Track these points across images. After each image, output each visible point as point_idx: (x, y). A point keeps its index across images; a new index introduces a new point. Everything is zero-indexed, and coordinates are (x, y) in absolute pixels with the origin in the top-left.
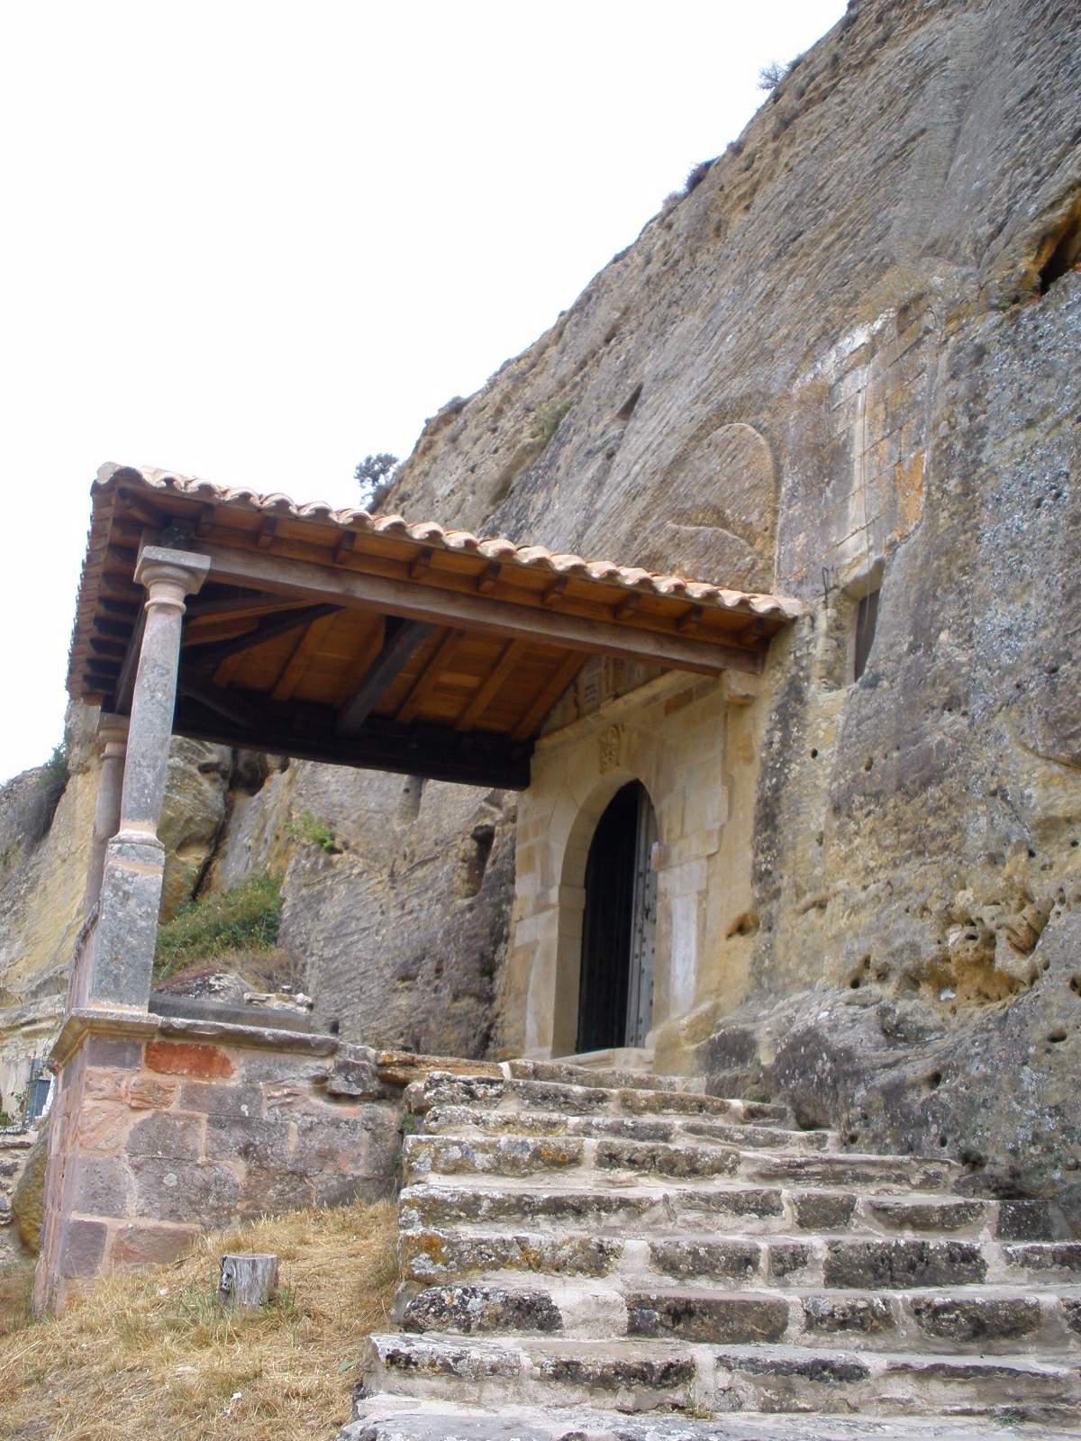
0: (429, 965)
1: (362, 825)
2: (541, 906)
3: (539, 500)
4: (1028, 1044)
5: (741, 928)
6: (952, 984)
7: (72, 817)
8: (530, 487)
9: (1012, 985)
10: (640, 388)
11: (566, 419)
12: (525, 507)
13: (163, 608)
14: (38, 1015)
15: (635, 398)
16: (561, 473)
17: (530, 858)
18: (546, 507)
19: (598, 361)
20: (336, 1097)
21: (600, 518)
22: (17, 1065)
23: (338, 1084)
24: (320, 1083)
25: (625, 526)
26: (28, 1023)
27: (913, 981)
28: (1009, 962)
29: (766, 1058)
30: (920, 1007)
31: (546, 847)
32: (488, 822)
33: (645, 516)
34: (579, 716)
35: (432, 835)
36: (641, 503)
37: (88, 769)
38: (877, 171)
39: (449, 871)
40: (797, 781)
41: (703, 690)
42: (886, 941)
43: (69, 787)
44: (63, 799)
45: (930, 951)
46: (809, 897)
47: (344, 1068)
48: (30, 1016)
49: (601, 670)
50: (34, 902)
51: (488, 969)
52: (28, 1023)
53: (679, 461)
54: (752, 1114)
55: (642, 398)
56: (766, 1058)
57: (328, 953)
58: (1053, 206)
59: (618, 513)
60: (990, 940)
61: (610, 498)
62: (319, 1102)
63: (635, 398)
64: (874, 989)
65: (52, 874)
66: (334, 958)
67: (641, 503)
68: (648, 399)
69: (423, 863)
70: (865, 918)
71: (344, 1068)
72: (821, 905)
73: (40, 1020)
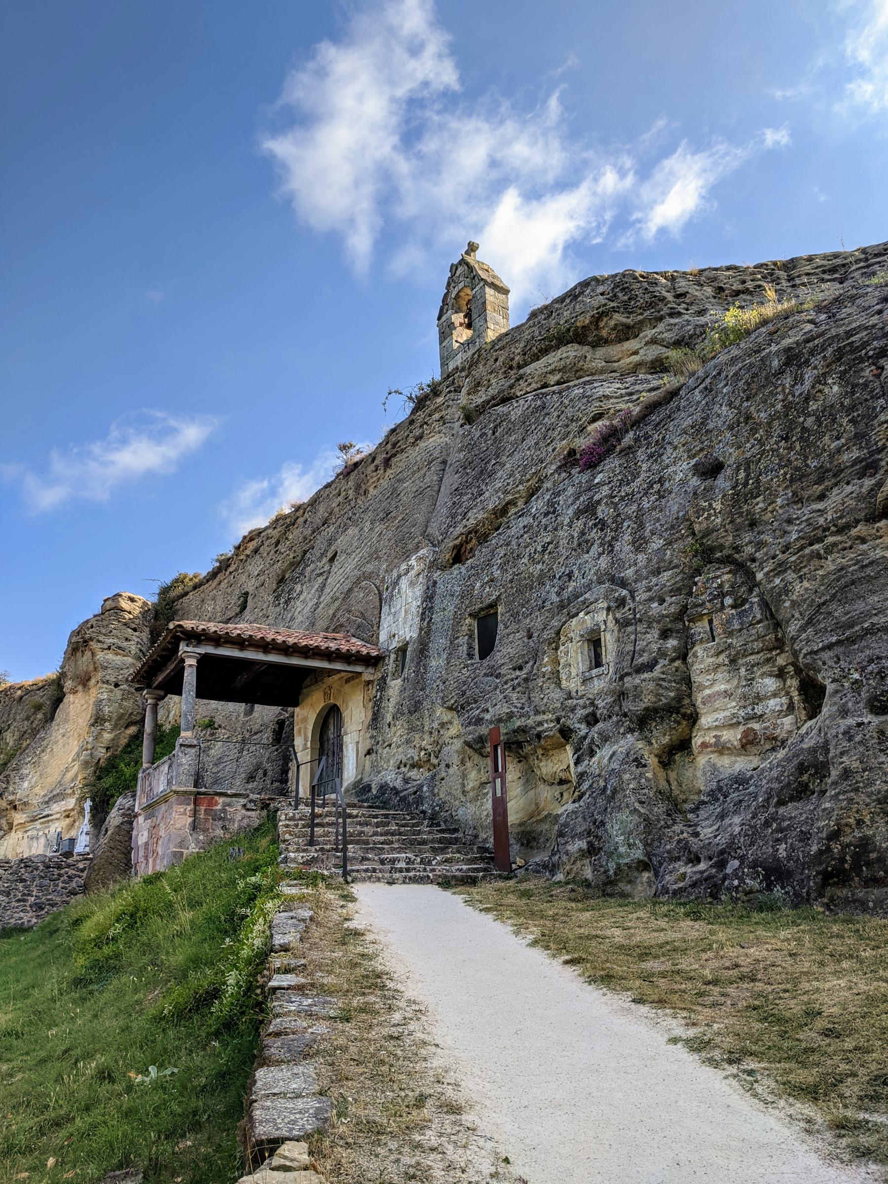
0: (261, 772)
1: (227, 717)
2: (305, 748)
3: (298, 588)
4: (809, 870)
5: (369, 753)
6: (420, 767)
7: (68, 714)
8: (294, 580)
9: (434, 767)
10: (336, 553)
11: (308, 555)
12: (291, 590)
13: (190, 666)
14: (50, 812)
15: (335, 555)
16: (307, 579)
17: (300, 731)
18: (301, 592)
19: (320, 533)
20: (248, 810)
21: (321, 606)
22: (37, 838)
23: (248, 806)
24: (244, 806)
25: (331, 612)
26: (44, 817)
27: (413, 766)
28: (434, 761)
29: (374, 791)
30: (413, 774)
31: (306, 728)
32: (282, 717)
33: (338, 609)
34: (316, 682)
35: (259, 722)
36: (337, 604)
37: (77, 692)
38: (415, 497)
39: (267, 736)
40: (384, 708)
41: (357, 678)
42: (406, 756)
43: (65, 700)
44: (61, 706)
45: (416, 758)
46: (386, 744)
47: (251, 801)
48: (45, 813)
49: (353, 890)
50: (45, 757)
51: (285, 771)
52: (44, 817)
53: (350, 590)
54: (370, 807)
55: (337, 557)
56: (374, 791)
57: (215, 770)
58: (457, 538)
59: (328, 605)
60: (430, 755)
61: (326, 599)
62: (244, 811)
63: (335, 555)
64: (403, 769)
65: (56, 742)
66: (218, 772)
67: (337, 604)
68: (341, 558)
69: (256, 733)
70: (400, 750)
71: (251, 801)
72: (390, 745)
73: (51, 815)
